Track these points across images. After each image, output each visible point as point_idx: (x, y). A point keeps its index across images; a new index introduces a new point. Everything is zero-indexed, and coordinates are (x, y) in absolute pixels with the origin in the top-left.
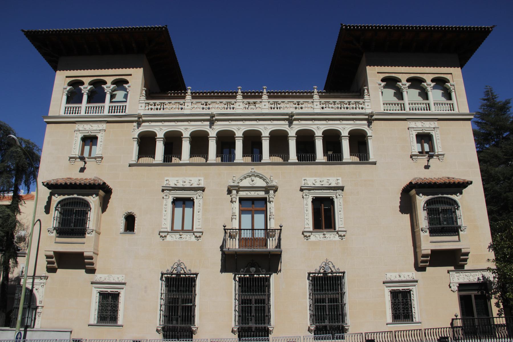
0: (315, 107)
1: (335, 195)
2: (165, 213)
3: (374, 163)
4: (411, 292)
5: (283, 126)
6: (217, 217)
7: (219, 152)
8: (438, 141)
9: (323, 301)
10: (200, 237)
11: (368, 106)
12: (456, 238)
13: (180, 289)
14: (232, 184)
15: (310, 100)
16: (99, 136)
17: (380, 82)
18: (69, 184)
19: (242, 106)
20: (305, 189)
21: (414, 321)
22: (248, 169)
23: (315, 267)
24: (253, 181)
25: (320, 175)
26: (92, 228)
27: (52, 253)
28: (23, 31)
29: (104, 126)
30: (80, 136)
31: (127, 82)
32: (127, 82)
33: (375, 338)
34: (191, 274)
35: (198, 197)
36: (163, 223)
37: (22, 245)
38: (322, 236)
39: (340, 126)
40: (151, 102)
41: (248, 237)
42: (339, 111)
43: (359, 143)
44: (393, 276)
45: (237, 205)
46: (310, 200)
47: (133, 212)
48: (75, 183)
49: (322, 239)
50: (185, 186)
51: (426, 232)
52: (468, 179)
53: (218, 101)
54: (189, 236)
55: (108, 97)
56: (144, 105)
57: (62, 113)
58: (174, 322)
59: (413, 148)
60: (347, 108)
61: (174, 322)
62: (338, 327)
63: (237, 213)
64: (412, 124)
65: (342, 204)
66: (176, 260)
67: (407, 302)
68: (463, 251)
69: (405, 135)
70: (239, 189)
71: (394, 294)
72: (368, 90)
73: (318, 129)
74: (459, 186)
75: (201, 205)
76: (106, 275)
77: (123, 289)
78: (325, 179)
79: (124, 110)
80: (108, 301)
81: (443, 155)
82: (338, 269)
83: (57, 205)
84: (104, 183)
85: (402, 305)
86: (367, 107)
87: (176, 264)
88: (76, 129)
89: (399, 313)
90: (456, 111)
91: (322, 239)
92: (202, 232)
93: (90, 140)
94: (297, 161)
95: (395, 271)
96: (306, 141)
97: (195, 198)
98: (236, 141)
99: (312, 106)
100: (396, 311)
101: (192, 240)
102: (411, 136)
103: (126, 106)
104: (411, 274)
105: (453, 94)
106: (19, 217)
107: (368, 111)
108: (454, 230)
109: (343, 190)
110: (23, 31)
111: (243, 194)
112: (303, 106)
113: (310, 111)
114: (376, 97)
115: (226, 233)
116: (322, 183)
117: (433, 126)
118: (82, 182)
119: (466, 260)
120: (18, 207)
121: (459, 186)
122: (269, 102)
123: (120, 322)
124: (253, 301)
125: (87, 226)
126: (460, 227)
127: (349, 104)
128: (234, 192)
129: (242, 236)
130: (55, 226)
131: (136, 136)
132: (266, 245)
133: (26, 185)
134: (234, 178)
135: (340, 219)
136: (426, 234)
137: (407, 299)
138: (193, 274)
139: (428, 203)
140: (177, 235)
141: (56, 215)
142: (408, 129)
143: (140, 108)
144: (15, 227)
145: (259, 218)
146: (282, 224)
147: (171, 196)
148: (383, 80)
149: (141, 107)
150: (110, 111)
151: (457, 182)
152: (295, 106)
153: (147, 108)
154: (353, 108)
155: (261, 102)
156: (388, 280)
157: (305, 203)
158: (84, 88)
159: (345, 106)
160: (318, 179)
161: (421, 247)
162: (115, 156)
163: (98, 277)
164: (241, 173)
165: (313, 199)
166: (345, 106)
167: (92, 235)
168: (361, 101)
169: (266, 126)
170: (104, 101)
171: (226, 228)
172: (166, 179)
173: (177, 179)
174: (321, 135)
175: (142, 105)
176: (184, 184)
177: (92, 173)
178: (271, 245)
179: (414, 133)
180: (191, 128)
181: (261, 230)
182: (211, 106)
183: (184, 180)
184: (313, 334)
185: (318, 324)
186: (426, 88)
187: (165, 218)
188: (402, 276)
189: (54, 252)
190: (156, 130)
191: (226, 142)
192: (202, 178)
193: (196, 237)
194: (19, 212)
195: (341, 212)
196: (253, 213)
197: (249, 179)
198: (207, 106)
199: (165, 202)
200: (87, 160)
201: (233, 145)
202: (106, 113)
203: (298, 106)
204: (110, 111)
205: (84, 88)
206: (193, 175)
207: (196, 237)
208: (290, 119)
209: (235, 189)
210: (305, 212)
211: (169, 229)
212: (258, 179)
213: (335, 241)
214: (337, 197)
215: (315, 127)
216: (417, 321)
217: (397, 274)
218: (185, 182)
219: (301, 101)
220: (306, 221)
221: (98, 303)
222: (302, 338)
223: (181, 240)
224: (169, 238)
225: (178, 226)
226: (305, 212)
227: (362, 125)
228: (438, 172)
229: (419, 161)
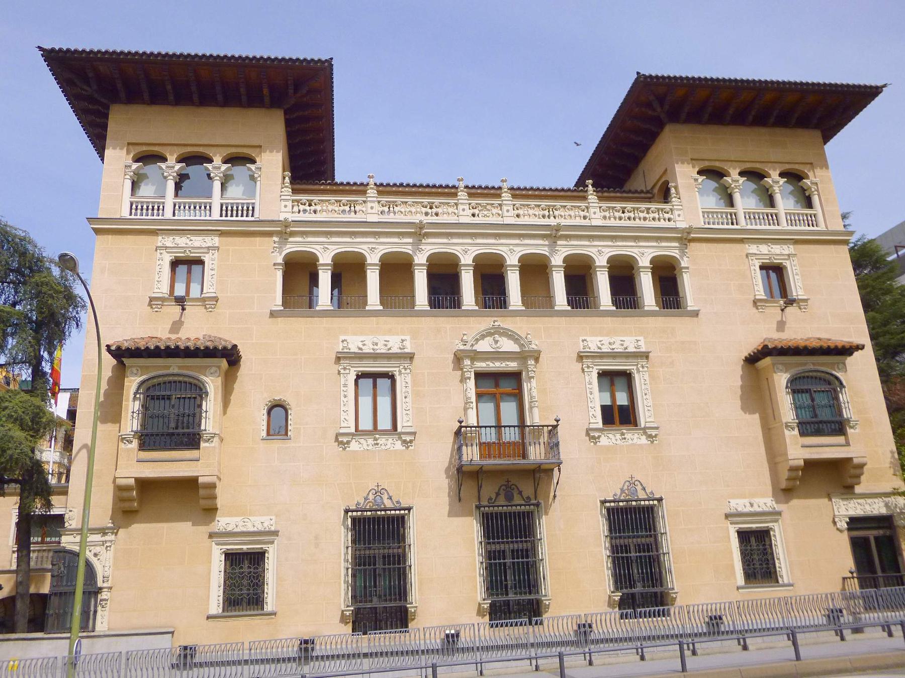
0: (461, 213)
1: (635, 367)
2: (345, 400)
3: (696, 314)
4: (772, 533)
5: (404, 246)
6: (439, 405)
7: (433, 290)
8: (796, 277)
9: (627, 549)
10: (411, 441)
11: (679, 215)
12: (841, 439)
13: (379, 540)
14: (462, 347)
15: (452, 201)
16: (207, 259)
18: (163, 348)
19: (377, 208)
20: (587, 357)
21: (780, 582)
22: (486, 322)
23: (612, 490)
24: (496, 342)
25: (607, 332)
26: (211, 431)
27: (132, 482)
28: (885, 86)
29: (216, 241)
30: (167, 258)
33: (594, 621)
34: (400, 510)
35: (403, 371)
36: (342, 419)
38: (618, 436)
39: (636, 250)
40: (304, 198)
41: (513, 439)
42: (618, 223)
44: (740, 504)
45: (471, 383)
46: (595, 376)
47: (283, 398)
48: (177, 347)
49: (619, 442)
50: (378, 351)
51: (793, 429)
53: (532, 203)
54: (390, 440)
55: (217, 185)
56: (290, 204)
57: (125, 213)
58: (375, 599)
59: (756, 288)
60: (645, 219)
61: (375, 599)
62: (530, 602)
63: (473, 399)
64: (753, 249)
65: (648, 382)
66: (372, 485)
67: (765, 549)
68: (855, 461)
69: (742, 268)
70: (475, 356)
71: (744, 536)
72: (676, 188)
73: (601, 255)
74: (846, 351)
75: (409, 385)
76: (238, 519)
77: (272, 543)
78: (617, 339)
79: (250, 212)
80: (241, 568)
81: (806, 300)
82: (652, 493)
83: (138, 389)
84: (235, 347)
85: (758, 554)
86: (678, 219)
87: (627, 483)
88: (160, 244)
89: (249, 590)
90: (822, 227)
91: (619, 442)
92: (414, 434)
93: (186, 264)
94: (381, 308)
95: (742, 496)
97: (397, 374)
98: (368, 271)
99: (500, 212)
100: (748, 565)
102: (752, 268)
103: (210, 203)
104: (765, 502)
105: (816, 199)
107: (682, 225)
108: (838, 427)
109: (647, 357)
110: (885, 86)
111: (482, 366)
112: (318, 208)
113: (452, 219)
114: (693, 201)
116: (613, 347)
117: (787, 252)
118: (191, 345)
119: (858, 476)
121: (846, 351)
122: (379, 202)
123: (269, 607)
124: (508, 554)
125: (203, 427)
126: (848, 420)
127: (648, 213)
128: (467, 362)
130: (135, 429)
131: (280, 260)
132: (524, 456)
134: (465, 338)
135: (646, 408)
136: (793, 433)
137: (764, 545)
138: (405, 509)
139: (792, 381)
142: (747, 256)
143: (283, 209)
145: (509, 410)
146: (560, 417)
147: (353, 370)
149: (286, 206)
150: (224, 212)
151: (840, 346)
152: (424, 210)
153: (296, 209)
154: (654, 219)
155: (364, 202)
156: (733, 511)
157: (587, 380)
158: (167, 167)
159: (642, 215)
160: (606, 340)
161: (786, 454)
162: (240, 295)
163: (223, 522)
164: (470, 328)
165: (598, 373)
166: (642, 215)
167: (213, 445)
168: (667, 207)
169: (511, 247)
170: (210, 196)
171: (463, 424)
172: (342, 338)
173: (362, 338)
174: (648, 264)
175: (287, 203)
176: (375, 347)
177: (197, 329)
178: (536, 453)
179: (757, 264)
180: (382, 247)
181: (490, 427)
182: (440, 210)
183: (375, 340)
184: (488, 617)
185: (625, 591)
186: (772, 186)
187: (345, 409)
188: (755, 506)
190: (316, 250)
192: (408, 338)
193: (404, 442)
195: (647, 396)
196: (497, 399)
197: (489, 340)
198: (313, 208)
199: (343, 381)
201: (314, 280)
202: (216, 215)
203: (430, 211)
204: (224, 212)
205: (167, 167)
206: (390, 332)
207: (404, 442)
208: (419, 232)
209: (467, 357)
210: (342, 398)
211: (353, 430)
212: (505, 339)
213: (640, 445)
214: (638, 371)
215: (594, 250)
216: (786, 581)
217: (746, 501)
218: (377, 344)
219: (437, 201)
220: (592, 412)
221: (223, 573)
222: (421, 630)
223: (378, 448)
224: (354, 446)
225: (366, 424)
226: (342, 398)
227: (671, 250)
228: (801, 329)
229: (767, 310)
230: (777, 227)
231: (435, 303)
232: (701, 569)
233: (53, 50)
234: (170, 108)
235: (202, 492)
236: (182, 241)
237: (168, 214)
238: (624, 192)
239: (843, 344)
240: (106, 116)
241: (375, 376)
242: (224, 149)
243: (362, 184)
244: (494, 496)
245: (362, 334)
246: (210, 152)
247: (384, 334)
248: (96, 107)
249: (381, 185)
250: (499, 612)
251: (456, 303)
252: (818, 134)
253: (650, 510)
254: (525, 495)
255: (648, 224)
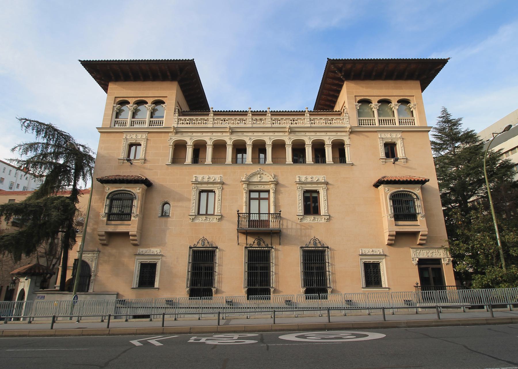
3: (352, 165)
17: (377, 103)
22: (256, 168)
25: (310, 174)
27: (103, 233)
29: (399, 135)
31: (163, 103)
32: (163, 103)
37: (79, 228)
40: (183, 118)
43: (339, 148)
44: (368, 251)
52: (427, 178)
71: (367, 266)
84: (146, 179)
85: (372, 275)
96: (319, 150)
101: (214, 221)
106: (77, 206)
115: (239, 216)
120: (77, 198)
123: (157, 285)
129: (251, 219)
130: (106, 212)
133: (83, 180)
140: (204, 218)
141: (107, 203)
144: (74, 213)
148: (359, 102)
162: (154, 159)
185: (307, 287)
189: (105, 232)
191: (239, 148)
194: (78, 202)
200: (132, 161)
206: (214, 173)
230: (394, 126)
231: (295, 161)
232: (345, 278)
233: (84, 61)
234: (404, 82)
235: (131, 238)
236: (388, 135)
237: (128, 125)
238: (333, 112)
239: (399, 178)
240: (108, 86)
241: (208, 191)
242: (151, 98)
243: (302, 111)
244: (252, 243)
245: (203, 174)
246: (129, 100)
247: (212, 174)
248: (337, 82)
249: (216, 111)
250: (251, 292)
251: (324, 161)
252: (417, 84)
253: (194, 252)
254: (266, 243)
255: (198, 126)
